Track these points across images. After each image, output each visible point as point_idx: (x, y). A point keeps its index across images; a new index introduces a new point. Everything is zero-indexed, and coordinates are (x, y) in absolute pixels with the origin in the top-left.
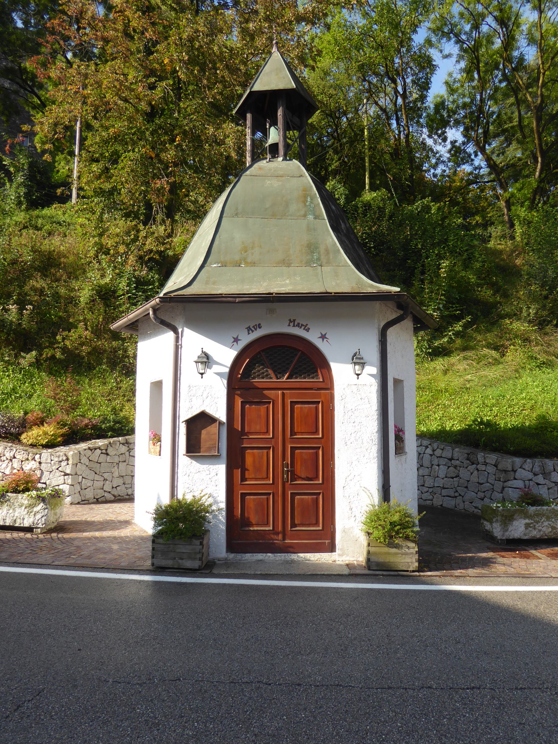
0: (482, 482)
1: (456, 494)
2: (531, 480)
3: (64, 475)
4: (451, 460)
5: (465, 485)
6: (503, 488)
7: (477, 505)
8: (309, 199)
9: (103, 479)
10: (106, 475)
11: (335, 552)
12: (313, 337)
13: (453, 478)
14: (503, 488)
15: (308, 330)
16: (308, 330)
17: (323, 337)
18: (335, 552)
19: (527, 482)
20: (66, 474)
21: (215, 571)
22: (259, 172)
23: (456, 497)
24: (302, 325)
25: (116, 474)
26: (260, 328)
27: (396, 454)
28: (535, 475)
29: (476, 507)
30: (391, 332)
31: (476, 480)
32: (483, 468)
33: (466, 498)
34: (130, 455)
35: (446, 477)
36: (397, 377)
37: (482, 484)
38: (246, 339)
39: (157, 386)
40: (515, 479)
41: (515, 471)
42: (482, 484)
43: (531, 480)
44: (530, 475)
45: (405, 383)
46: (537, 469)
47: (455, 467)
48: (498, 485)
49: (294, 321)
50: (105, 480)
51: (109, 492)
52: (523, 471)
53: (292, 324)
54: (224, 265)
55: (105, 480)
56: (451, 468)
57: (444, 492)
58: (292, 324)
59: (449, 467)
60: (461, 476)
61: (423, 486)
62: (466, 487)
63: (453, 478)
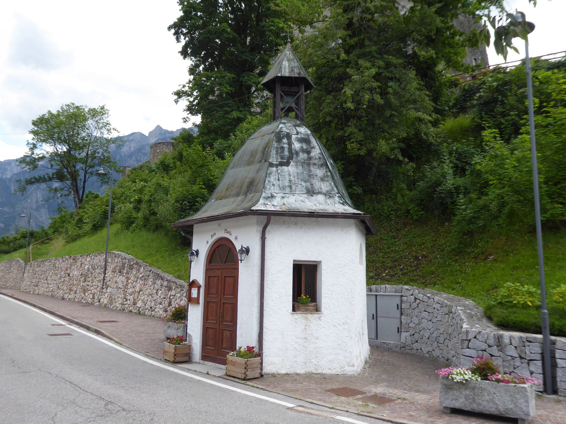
28: (489, 346)
38: (211, 241)
40: (468, 348)
46: (491, 341)
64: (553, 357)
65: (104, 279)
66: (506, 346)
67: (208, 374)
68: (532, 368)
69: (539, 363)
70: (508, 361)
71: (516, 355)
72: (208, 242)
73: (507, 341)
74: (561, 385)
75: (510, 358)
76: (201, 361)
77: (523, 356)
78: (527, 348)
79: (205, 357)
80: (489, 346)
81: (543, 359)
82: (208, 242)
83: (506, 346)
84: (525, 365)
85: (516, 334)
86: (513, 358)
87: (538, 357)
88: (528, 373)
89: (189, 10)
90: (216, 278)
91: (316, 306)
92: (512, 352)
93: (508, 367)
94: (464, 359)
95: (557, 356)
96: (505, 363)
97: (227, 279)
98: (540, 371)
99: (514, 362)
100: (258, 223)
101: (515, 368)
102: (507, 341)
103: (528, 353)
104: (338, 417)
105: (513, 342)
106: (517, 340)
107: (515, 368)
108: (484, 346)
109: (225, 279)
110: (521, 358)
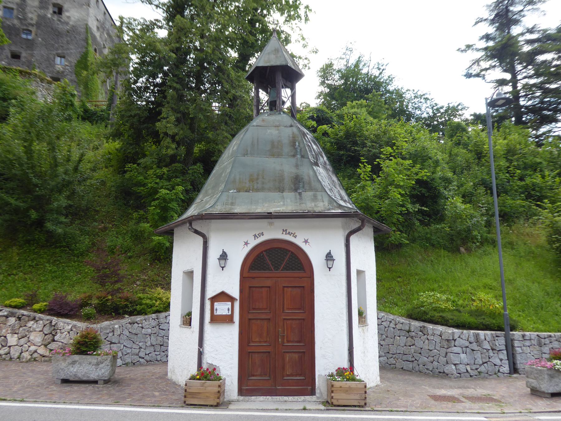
0: (431, 349)
1: (413, 359)
2: (468, 347)
3: (110, 344)
4: (409, 331)
5: (420, 352)
6: (447, 353)
7: (428, 367)
8: (297, 144)
9: (138, 347)
10: (141, 344)
11: (315, 395)
12: (298, 241)
13: (410, 346)
14: (447, 353)
15: (295, 237)
16: (295, 237)
17: (306, 241)
18: (315, 395)
19: (464, 349)
20: (112, 343)
21: (231, 407)
22: (262, 124)
23: (413, 361)
24: (292, 233)
25: (149, 344)
26: (263, 235)
27: (359, 323)
28: (470, 343)
29: (427, 369)
30: (353, 239)
31: (427, 347)
32: (432, 338)
33: (420, 362)
34: (284, 287)
35: (405, 346)
36: (359, 269)
37: (431, 351)
38: (253, 243)
39: (190, 274)
40: (455, 346)
41: (455, 340)
42: (431, 351)
43: (468, 347)
44: (467, 344)
45: (366, 273)
46: (472, 339)
47: (412, 337)
48: (443, 351)
49: (286, 230)
50: (140, 348)
51: (143, 358)
52: (461, 340)
53: (284, 233)
54: (239, 191)
55: (140, 348)
56: (409, 338)
57: (405, 357)
58: (284, 233)
59: (407, 337)
60: (416, 344)
61: (388, 353)
62: (420, 353)
63: (410, 346)
64: (513, 346)
65: (502, 286)
66: (482, 341)
67: (305, 409)
68: (501, 356)
69: (505, 352)
70: (485, 353)
71: (489, 348)
72: (246, 244)
73: (482, 337)
74: (519, 366)
75: (485, 351)
76: (241, 398)
77: (494, 348)
78: (496, 341)
79: (246, 388)
80: (470, 343)
81: (507, 350)
82: (246, 244)
83: (482, 341)
84: (496, 355)
85: (488, 332)
86: (488, 350)
87: (504, 348)
88: (499, 361)
89: (497, 4)
90: (264, 290)
91: (404, 316)
92: (487, 346)
93: (485, 358)
94: (453, 356)
95: (516, 345)
96: (483, 355)
97: (285, 289)
98: (506, 358)
99: (489, 353)
100: (344, 228)
101: (489, 358)
102: (482, 337)
103: (498, 345)
104: (537, 418)
105: (487, 338)
106: (490, 336)
107: (489, 358)
108: (467, 344)
109: (283, 290)
110: (493, 349)
